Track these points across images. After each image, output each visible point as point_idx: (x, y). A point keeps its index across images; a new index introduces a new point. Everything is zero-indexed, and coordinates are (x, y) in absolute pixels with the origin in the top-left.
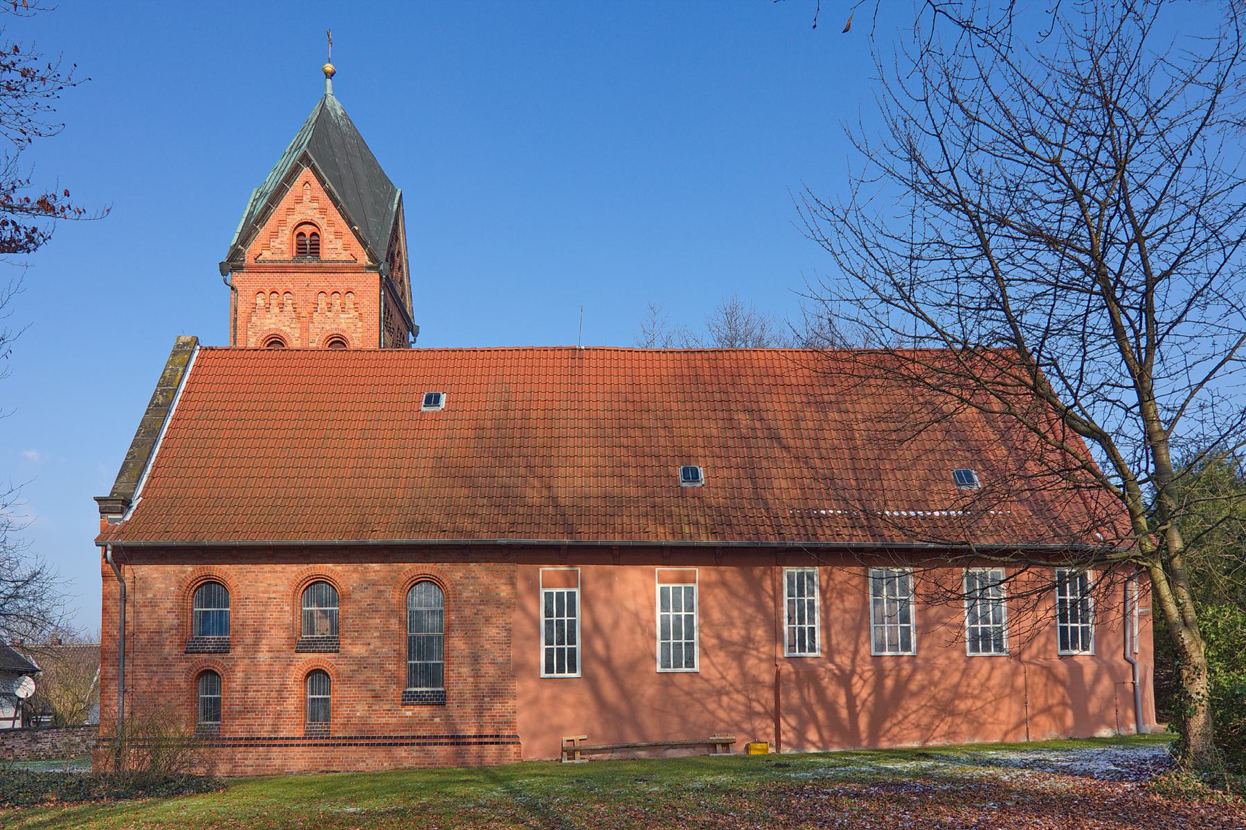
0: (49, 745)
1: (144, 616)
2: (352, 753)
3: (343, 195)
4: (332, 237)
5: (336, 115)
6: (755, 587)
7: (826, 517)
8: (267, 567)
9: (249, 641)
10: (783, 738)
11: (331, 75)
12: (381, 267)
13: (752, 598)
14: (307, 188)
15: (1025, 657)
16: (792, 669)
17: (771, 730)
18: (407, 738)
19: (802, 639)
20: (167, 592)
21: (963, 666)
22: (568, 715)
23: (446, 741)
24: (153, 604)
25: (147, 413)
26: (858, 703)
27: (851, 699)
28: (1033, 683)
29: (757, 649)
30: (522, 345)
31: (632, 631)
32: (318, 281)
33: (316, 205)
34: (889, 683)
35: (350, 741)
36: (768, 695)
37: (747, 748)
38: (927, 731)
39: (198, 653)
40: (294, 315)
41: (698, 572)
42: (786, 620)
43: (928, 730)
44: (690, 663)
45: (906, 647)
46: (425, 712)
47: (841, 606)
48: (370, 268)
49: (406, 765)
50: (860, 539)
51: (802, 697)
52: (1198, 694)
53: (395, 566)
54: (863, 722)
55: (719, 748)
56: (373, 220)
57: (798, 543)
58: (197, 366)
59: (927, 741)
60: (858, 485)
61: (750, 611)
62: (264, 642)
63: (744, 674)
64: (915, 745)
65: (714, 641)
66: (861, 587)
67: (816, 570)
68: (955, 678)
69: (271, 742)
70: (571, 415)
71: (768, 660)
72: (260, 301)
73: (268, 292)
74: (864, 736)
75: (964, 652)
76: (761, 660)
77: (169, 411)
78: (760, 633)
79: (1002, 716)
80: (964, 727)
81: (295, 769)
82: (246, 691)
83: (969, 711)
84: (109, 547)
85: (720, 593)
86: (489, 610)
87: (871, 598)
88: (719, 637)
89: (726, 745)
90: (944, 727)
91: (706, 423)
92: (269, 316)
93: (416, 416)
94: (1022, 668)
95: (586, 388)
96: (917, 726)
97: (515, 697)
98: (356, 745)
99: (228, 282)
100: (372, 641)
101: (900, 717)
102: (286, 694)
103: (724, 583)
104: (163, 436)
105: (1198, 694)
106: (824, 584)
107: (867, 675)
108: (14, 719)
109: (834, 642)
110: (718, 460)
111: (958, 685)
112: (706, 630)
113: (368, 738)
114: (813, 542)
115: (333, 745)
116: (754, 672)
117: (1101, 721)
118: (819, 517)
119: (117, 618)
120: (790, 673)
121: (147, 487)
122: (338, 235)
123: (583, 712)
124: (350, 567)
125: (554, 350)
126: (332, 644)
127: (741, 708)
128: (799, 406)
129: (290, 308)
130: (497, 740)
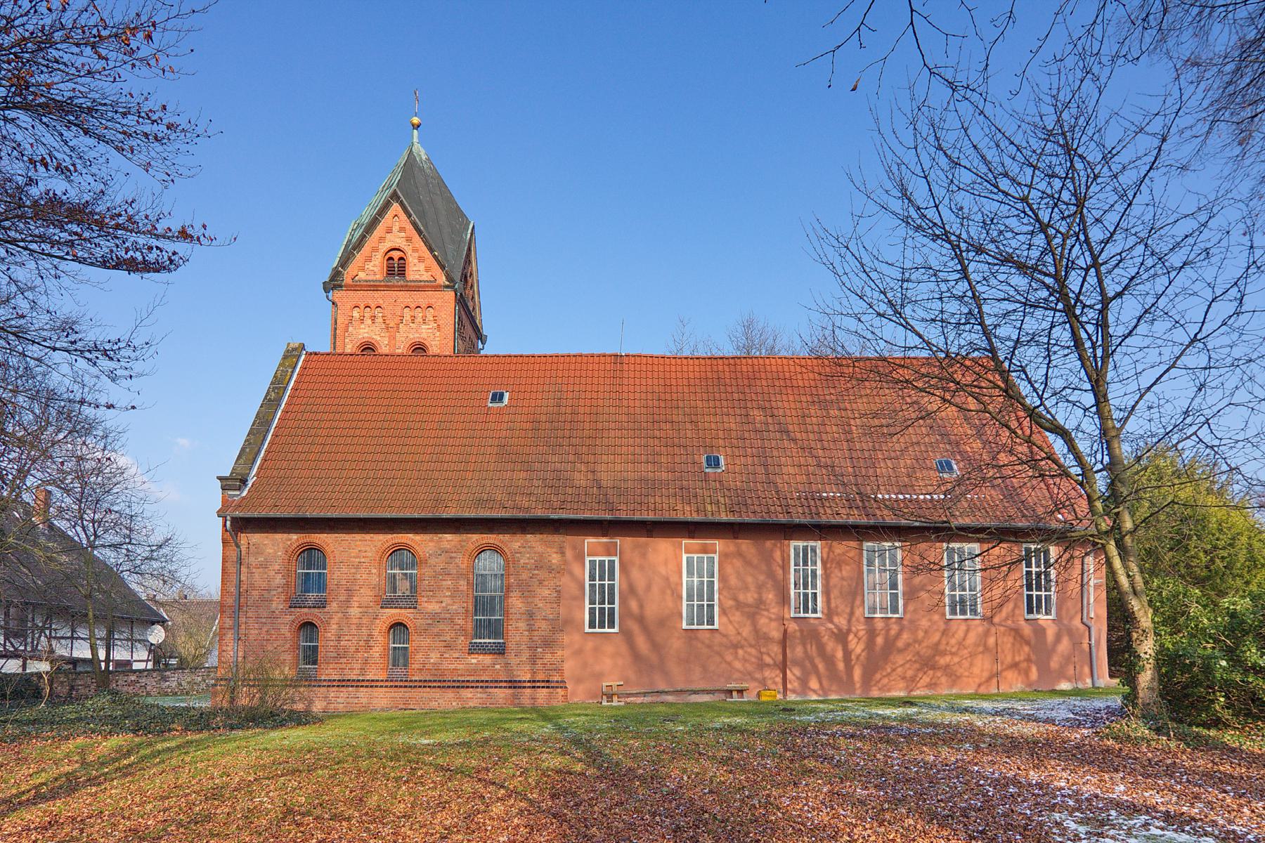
0: (175, 683)
2: (425, 693)
3: (426, 226)
6: (767, 558)
8: (358, 537)
10: (789, 686)
12: (456, 286)
13: (764, 567)
15: (996, 620)
16: (797, 628)
17: (779, 680)
18: (473, 681)
21: (942, 626)
22: (607, 663)
23: (505, 684)
26: (853, 657)
27: (847, 654)
31: (663, 592)
32: (405, 298)
35: (424, 684)
36: (776, 649)
37: (759, 695)
38: (911, 682)
40: (383, 326)
41: (718, 544)
42: (792, 586)
43: (913, 681)
44: (711, 622)
45: (895, 610)
46: (488, 659)
47: (839, 575)
48: (447, 287)
49: (471, 704)
50: (856, 518)
51: (806, 652)
52: (1146, 653)
53: (464, 536)
54: (857, 673)
55: (735, 694)
57: (803, 520)
58: (304, 368)
59: (912, 691)
61: (762, 578)
62: (355, 599)
63: (756, 631)
64: (902, 694)
65: (731, 603)
67: (818, 544)
68: (936, 637)
69: (358, 684)
70: (612, 410)
72: (356, 314)
73: (362, 307)
74: (858, 685)
75: (944, 614)
76: (771, 619)
78: (770, 596)
79: (976, 670)
80: (943, 679)
83: (947, 666)
84: (228, 518)
85: (738, 563)
86: (542, 574)
88: (735, 599)
89: (740, 692)
90: (926, 680)
92: (363, 326)
94: (993, 630)
96: (904, 678)
98: (430, 687)
99: (330, 298)
100: (444, 599)
102: (372, 643)
103: (740, 554)
105: (1146, 653)
107: (861, 633)
108: (147, 661)
109: (833, 605)
111: (938, 643)
112: (725, 593)
113: (440, 681)
114: (816, 520)
117: (1062, 675)
118: (821, 499)
119: (234, 578)
121: (260, 468)
122: (421, 259)
124: (427, 537)
126: (411, 601)
127: (753, 660)
129: (380, 320)
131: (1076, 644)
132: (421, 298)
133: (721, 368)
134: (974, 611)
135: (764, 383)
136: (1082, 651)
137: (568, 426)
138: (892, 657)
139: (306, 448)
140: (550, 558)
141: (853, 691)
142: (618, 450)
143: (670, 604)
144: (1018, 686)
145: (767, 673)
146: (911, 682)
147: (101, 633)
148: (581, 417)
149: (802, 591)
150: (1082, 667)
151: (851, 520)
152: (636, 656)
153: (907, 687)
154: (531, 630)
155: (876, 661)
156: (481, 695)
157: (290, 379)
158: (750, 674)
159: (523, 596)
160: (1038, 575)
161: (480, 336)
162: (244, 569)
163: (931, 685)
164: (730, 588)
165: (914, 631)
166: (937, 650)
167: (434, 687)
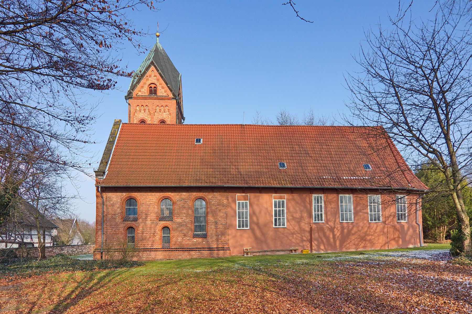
0: (66, 251)
1: (110, 209)
2: (177, 253)
3: (164, 75)
4: (161, 88)
5: (160, 49)
6: (304, 201)
7: (326, 178)
8: (150, 194)
9: (144, 217)
10: (313, 248)
11: (158, 36)
12: (177, 98)
13: (303, 204)
14: (152, 72)
15: (387, 223)
16: (316, 227)
17: (309, 246)
18: (195, 248)
19: (319, 217)
20: (117, 202)
21: (368, 225)
22: (245, 241)
23: (207, 249)
24: (113, 205)
25: (107, 144)
26: (336, 237)
27: (334, 236)
28: (390, 231)
29: (304, 220)
30: (221, 124)
31: (265, 214)
32: (157, 102)
33: (155, 78)
34: (346, 231)
35: (176, 249)
36: (308, 234)
37: (302, 251)
38: (357, 246)
39: (127, 221)
40: (149, 113)
41: (286, 196)
42: (313, 211)
43: (358, 245)
44: (284, 225)
45: (351, 220)
46: (200, 240)
47: (330, 206)
48: (173, 98)
49: (195, 257)
50: (337, 186)
51: (319, 235)
52: (467, 233)
53: (190, 193)
54: (338, 243)
55: (293, 251)
56: (173, 83)
57: (318, 186)
58: (122, 129)
59: (357, 249)
60: (334, 169)
61: (302, 208)
62: (149, 218)
63: (300, 228)
64: (354, 250)
65: (291, 217)
66: (337, 200)
67: (322, 195)
68: (366, 229)
69: (151, 250)
70: (242, 146)
71: (307, 224)
72: (138, 108)
73: (140, 106)
74: (338, 247)
75: (368, 221)
76: (306, 224)
77: (114, 143)
78: (305, 215)
79: (380, 241)
80: (369, 245)
81: (159, 258)
82: (143, 234)
83: (370, 240)
84: (100, 187)
85: (293, 203)
86: (220, 207)
87: (340, 204)
88: (292, 216)
89: (295, 250)
90: (363, 245)
91: (285, 149)
92: (141, 113)
93: (193, 146)
94: (386, 226)
95: (246, 137)
96: (354, 244)
97: (229, 235)
98: (178, 251)
99: (128, 102)
100: (183, 217)
101: (349, 242)
102: (156, 234)
103: (294, 199)
104: (113, 151)
105: (467, 233)
106: (325, 200)
107: (339, 228)
108: (50, 243)
109: (328, 218)
110: (290, 160)
111: (367, 231)
112: (289, 214)
113: (182, 248)
114: (323, 186)
115: (171, 251)
116: (303, 227)
117: (410, 242)
118: (323, 179)
119: (101, 210)
120: (315, 228)
121: (109, 168)
122: (163, 88)
123: (250, 240)
124: (176, 194)
125: (235, 125)
126: (170, 218)
127: (299, 239)
128: (314, 144)
129: (147, 111)
130: (223, 249)
131: (415, 231)
132: (163, 103)
133: (281, 130)
134: (379, 220)
135: (298, 136)
136: (417, 233)
137: (226, 151)
138: (350, 237)
139: (126, 160)
140: (223, 201)
141: (336, 249)
142: (246, 160)
143: (268, 218)
144: (395, 247)
145: (305, 243)
146: (357, 246)
147: (41, 232)
148: (231, 148)
149: (317, 213)
150: (416, 239)
151: (336, 187)
152: (256, 238)
153: (356, 248)
154: (216, 229)
155: (344, 238)
156: (198, 253)
157: (117, 133)
158: (298, 244)
159: (213, 216)
160: (279, 211)
161: (184, 119)
162: (105, 207)
163: (364, 247)
164: (290, 212)
165: (358, 227)
166: (366, 234)
167: (180, 251)
